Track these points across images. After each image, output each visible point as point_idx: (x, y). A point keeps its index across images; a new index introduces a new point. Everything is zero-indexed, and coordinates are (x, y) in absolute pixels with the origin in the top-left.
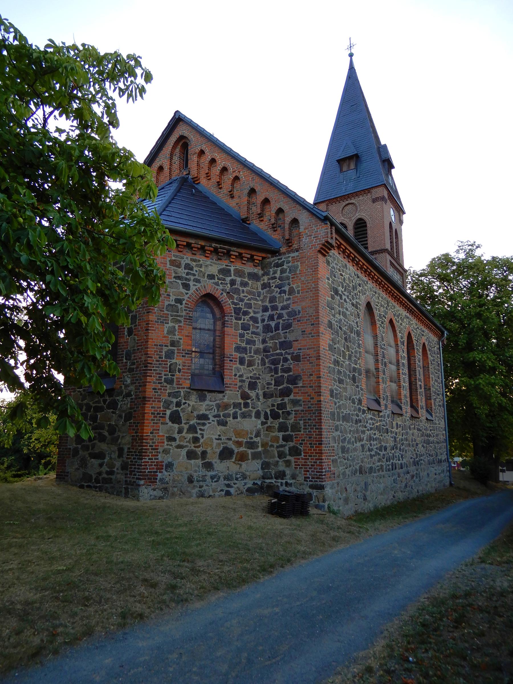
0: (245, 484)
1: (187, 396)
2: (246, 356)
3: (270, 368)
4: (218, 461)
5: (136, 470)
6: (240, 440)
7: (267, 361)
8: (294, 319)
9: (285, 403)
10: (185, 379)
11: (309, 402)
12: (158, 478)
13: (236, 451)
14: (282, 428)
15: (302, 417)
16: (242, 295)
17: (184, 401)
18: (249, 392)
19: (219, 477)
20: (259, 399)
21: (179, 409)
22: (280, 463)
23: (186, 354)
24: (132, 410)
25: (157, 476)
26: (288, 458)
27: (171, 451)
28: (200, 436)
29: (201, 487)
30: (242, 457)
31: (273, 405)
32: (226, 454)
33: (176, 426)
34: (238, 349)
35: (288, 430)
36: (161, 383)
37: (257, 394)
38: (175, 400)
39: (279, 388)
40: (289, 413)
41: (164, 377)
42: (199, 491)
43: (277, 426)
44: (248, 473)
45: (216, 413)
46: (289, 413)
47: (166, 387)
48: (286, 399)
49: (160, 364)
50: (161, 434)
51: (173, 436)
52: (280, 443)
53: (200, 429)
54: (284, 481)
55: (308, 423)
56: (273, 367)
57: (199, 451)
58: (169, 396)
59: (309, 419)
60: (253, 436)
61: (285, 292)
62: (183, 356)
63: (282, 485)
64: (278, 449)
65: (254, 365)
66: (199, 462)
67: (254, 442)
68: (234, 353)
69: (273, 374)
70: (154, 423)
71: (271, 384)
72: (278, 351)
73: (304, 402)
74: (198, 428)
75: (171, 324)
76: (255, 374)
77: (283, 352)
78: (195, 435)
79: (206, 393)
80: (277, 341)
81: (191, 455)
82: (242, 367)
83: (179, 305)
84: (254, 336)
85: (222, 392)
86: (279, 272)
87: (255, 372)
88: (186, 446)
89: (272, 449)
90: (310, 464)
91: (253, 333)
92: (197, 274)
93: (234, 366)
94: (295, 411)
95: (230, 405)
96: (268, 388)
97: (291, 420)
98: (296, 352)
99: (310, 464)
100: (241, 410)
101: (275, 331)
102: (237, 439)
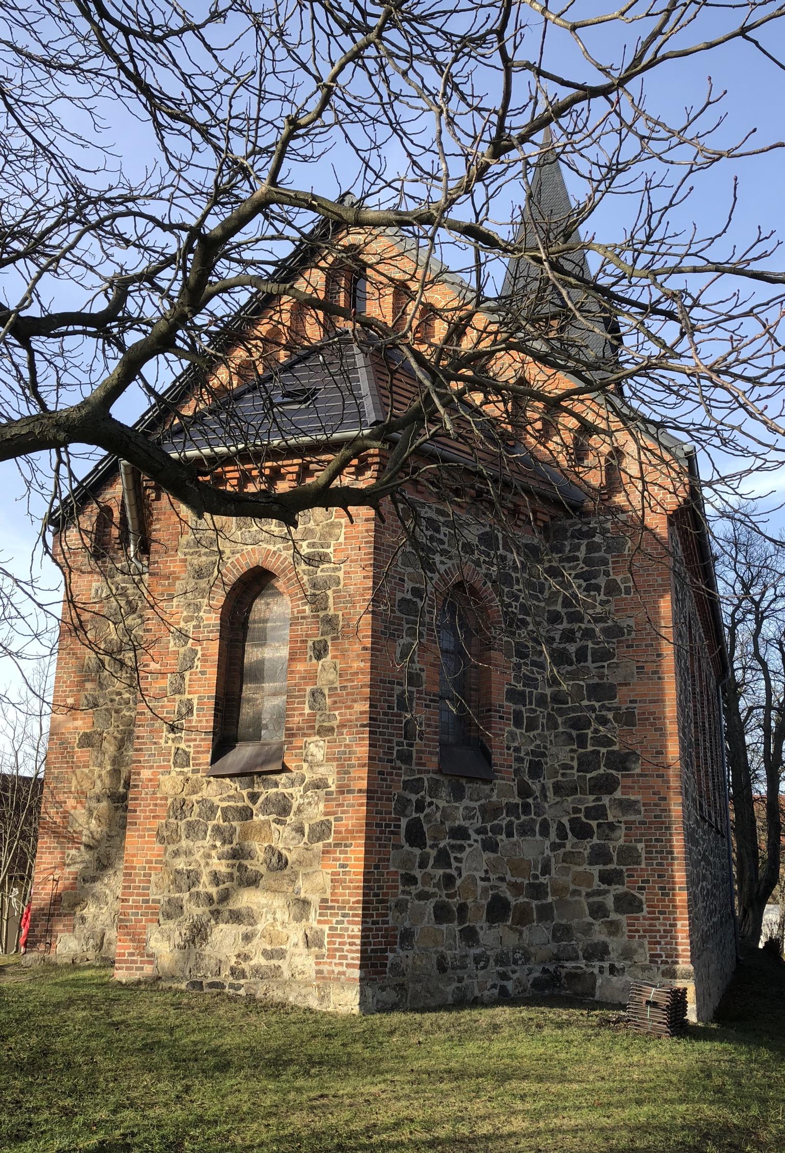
0: (530, 971)
1: (434, 791)
2: (523, 709)
3: (570, 736)
4: (485, 925)
5: (347, 947)
6: (519, 880)
7: (560, 720)
8: (619, 642)
9: (604, 806)
10: (430, 753)
11: (655, 805)
12: (389, 963)
13: (513, 903)
14: (600, 855)
15: (642, 835)
16: (516, 587)
17: (428, 799)
18: (530, 782)
19: (487, 961)
20: (545, 797)
21: (422, 816)
22: (597, 928)
23: (431, 701)
24: (331, 818)
25: (387, 958)
26: (614, 916)
27: (409, 905)
28: (455, 873)
29: (460, 980)
30: (523, 917)
31: (576, 810)
32: (498, 910)
33: (417, 851)
34: (515, 696)
35: (610, 861)
36: (390, 761)
37: (543, 786)
38: (414, 797)
39: (589, 776)
40: (612, 827)
41: (396, 748)
42: (458, 988)
43: (586, 853)
44: (532, 950)
45: (479, 825)
46: (612, 827)
47: (400, 769)
48: (606, 800)
49: (389, 721)
50: (392, 869)
51: (413, 873)
52: (595, 888)
53: (455, 858)
54: (606, 965)
55: (655, 847)
56: (574, 733)
57: (454, 902)
58: (405, 789)
59: (657, 840)
60: (538, 873)
61: (597, 588)
62: (427, 706)
63: (601, 972)
64: (591, 900)
65: (537, 728)
66: (455, 927)
67: (542, 884)
68: (505, 703)
69: (575, 747)
70: (380, 846)
71: (572, 768)
72: (585, 703)
73: (644, 805)
74: (452, 855)
75: (406, 640)
76: (538, 746)
77: (597, 705)
78: (448, 871)
79: (464, 781)
80: (582, 683)
81: (442, 913)
82: (518, 731)
83: (418, 600)
84: (535, 669)
85: (487, 781)
86: (583, 548)
87: (538, 742)
88: (434, 895)
89: (577, 898)
90: (662, 928)
91: (534, 664)
92: (446, 539)
93: (507, 729)
94: (626, 823)
95: (502, 809)
96: (563, 775)
97: (620, 839)
98: (624, 707)
99: (662, 928)
100: (518, 818)
101: (579, 661)
102: (513, 880)
